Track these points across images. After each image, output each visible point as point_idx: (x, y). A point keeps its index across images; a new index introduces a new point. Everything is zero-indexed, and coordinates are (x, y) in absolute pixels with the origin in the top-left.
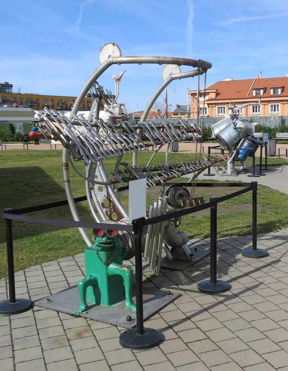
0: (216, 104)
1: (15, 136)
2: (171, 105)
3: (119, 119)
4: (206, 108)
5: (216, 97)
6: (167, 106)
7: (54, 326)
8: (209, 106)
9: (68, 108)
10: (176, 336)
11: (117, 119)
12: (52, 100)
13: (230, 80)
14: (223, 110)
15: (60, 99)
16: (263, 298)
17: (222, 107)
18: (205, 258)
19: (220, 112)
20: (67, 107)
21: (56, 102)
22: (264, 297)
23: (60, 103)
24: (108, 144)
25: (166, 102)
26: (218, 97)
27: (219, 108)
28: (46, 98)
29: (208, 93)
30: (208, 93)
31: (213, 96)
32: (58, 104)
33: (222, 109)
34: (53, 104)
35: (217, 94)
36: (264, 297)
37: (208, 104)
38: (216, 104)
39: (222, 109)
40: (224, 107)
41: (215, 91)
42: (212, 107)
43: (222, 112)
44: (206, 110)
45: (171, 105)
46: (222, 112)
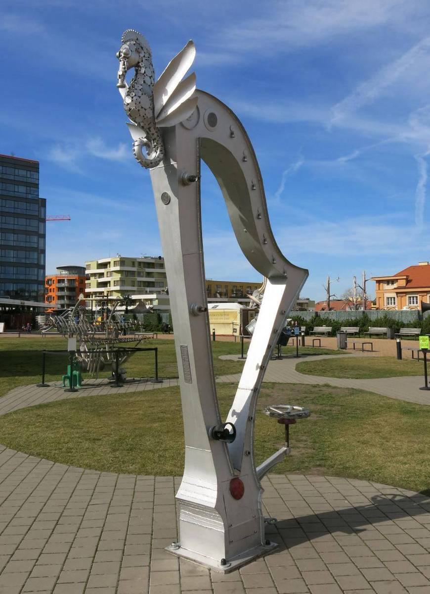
0: (406, 293)
1: (160, 326)
2: (334, 295)
3: (252, 312)
4: (394, 298)
5: (406, 285)
6: (329, 297)
7: (140, 565)
8: (398, 295)
9: (243, 296)
10: (368, 586)
11: (249, 312)
12: (226, 286)
13: (426, 264)
14: (393, 301)
15: (234, 285)
16: (392, 575)
17: (413, 297)
18: (12, 558)
19: (415, 303)
20: (242, 295)
21: (230, 288)
22: (393, 574)
23: (234, 289)
24: (136, 346)
25: (329, 293)
26: (409, 285)
27: (410, 297)
28: (226, 284)
29: (397, 280)
30: (397, 280)
31: (403, 283)
32: (233, 291)
33: (413, 299)
34: (227, 291)
35: (408, 281)
36: (393, 574)
37: (397, 293)
38: (406, 293)
39: (413, 299)
40: (417, 297)
41: (405, 277)
42: (402, 297)
43: (413, 303)
44: (394, 300)
45: (334, 295)
46: (413, 303)
